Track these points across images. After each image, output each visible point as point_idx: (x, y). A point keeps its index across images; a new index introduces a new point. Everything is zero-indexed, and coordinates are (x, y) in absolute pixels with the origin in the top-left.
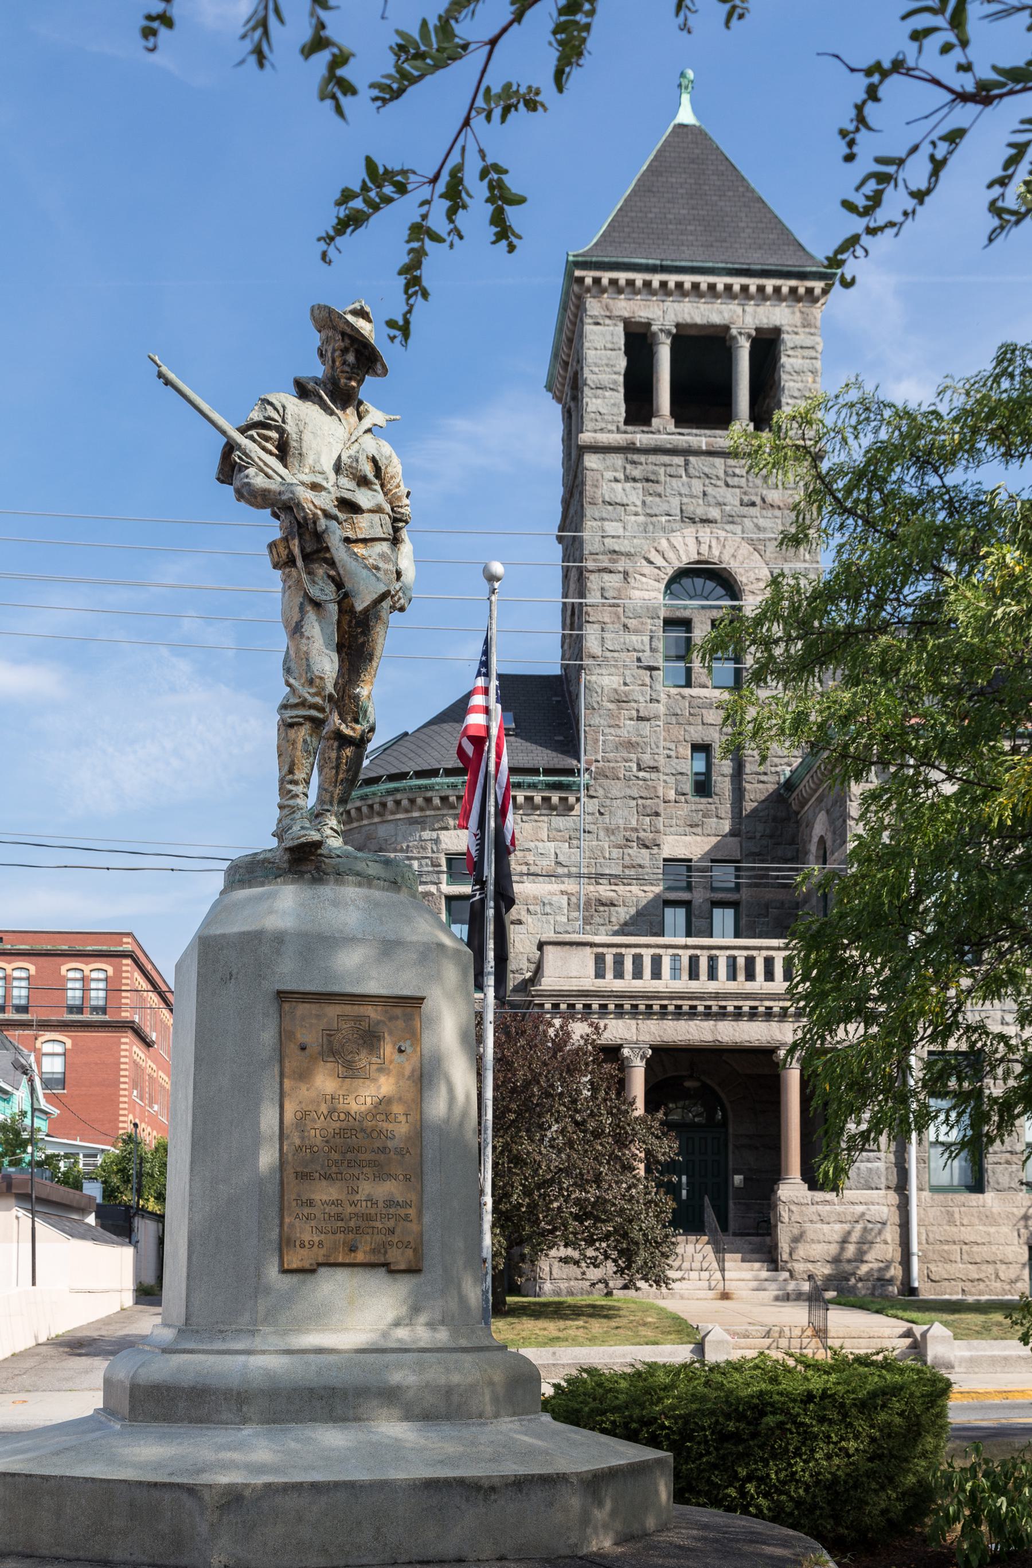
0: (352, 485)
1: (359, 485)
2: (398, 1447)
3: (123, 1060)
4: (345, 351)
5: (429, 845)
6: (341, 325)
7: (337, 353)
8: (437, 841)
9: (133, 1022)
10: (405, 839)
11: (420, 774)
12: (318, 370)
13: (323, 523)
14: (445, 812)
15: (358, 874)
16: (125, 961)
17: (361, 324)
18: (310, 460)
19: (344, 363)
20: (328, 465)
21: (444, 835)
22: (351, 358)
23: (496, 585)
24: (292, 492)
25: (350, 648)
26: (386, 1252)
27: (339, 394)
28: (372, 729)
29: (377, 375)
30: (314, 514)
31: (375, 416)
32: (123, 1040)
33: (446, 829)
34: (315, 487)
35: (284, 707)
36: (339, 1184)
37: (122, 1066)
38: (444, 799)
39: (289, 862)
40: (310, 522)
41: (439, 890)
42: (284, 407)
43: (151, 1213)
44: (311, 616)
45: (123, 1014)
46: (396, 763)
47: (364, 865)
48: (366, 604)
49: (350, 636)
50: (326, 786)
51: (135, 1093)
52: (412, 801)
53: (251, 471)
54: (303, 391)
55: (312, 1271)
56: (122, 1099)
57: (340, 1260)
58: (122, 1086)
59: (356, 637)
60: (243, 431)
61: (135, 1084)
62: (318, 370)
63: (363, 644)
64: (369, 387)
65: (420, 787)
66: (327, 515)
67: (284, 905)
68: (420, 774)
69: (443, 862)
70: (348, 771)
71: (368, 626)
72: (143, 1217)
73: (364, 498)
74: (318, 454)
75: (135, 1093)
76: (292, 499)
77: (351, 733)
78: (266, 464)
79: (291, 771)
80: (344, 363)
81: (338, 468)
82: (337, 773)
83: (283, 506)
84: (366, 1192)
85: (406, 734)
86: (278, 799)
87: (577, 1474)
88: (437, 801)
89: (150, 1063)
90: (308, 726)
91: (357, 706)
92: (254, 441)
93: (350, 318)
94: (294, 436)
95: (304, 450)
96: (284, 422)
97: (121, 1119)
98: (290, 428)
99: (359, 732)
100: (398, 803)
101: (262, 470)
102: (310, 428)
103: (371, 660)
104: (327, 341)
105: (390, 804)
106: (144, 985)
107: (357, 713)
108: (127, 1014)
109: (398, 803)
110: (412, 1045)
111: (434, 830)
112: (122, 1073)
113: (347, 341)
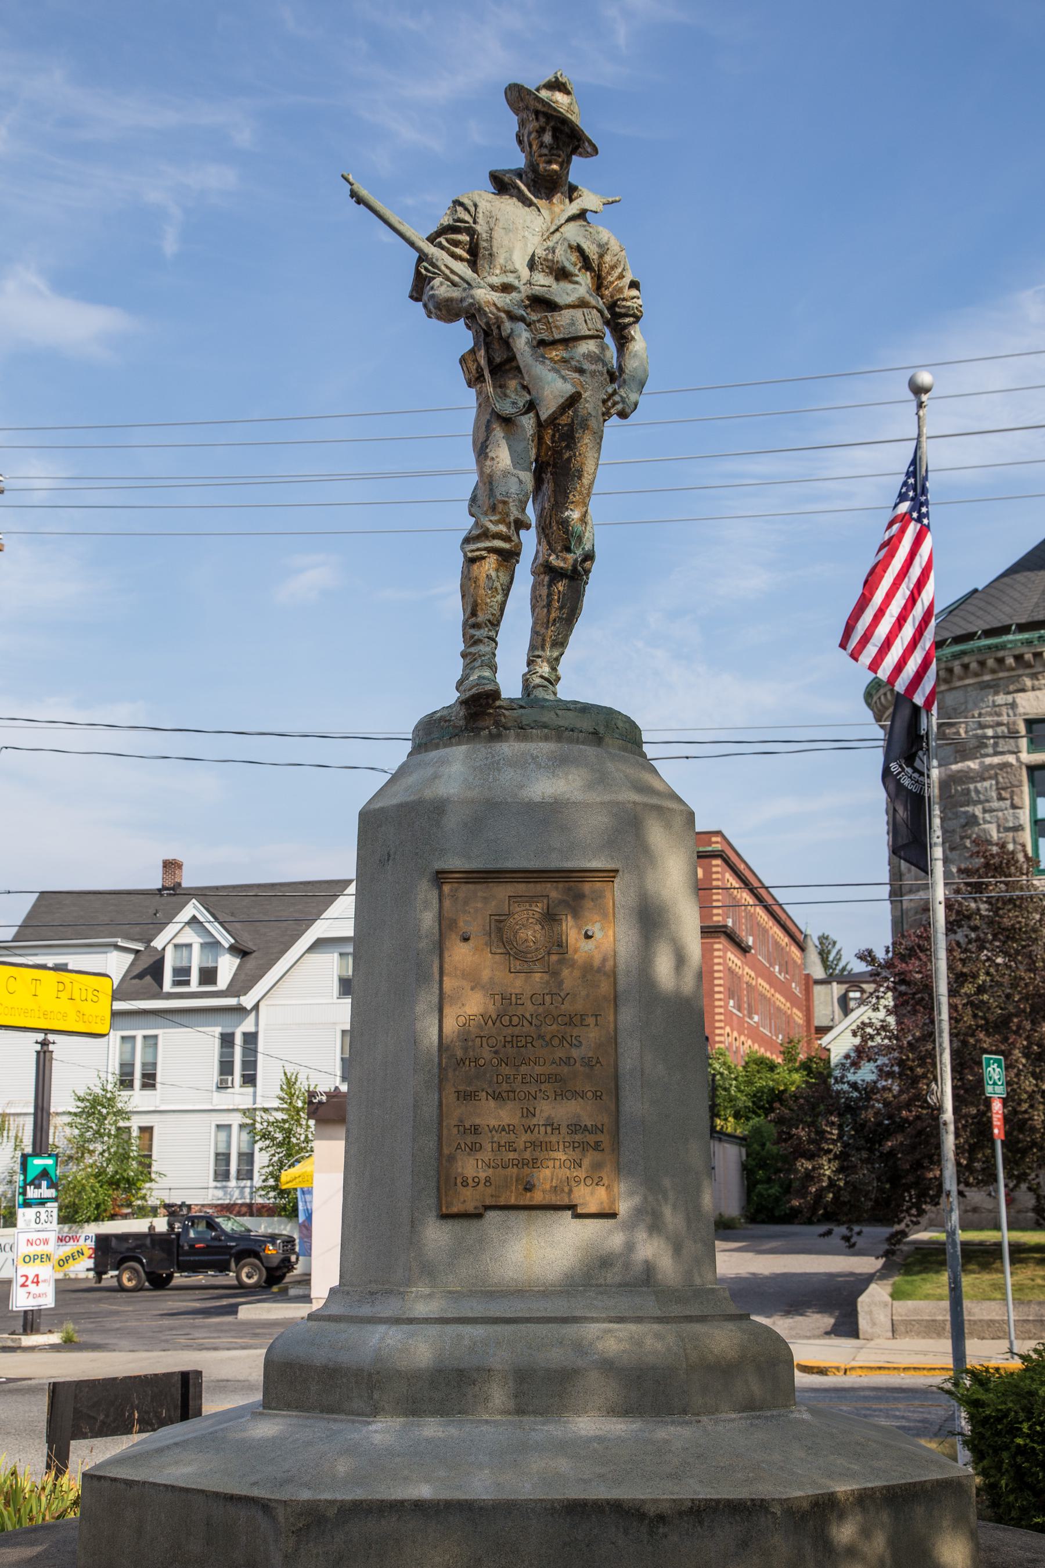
0: (549, 280)
1: (557, 279)
2: (589, 1447)
3: (716, 968)
4: (541, 131)
5: (1004, 710)
6: (533, 104)
7: (533, 136)
8: (1013, 705)
9: (726, 926)
10: (976, 705)
11: (989, 633)
12: (518, 160)
13: (507, 326)
14: (1020, 672)
15: (545, 726)
16: (715, 862)
17: (560, 97)
18: (501, 260)
19: (542, 145)
20: (520, 263)
21: (1020, 698)
22: (547, 138)
23: (924, 398)
24: (472, 297)
25: (554, 466)
26: (571, 1191)
27: (543, 182)
28: (589, 557)
29: (588, 155)
30: (497, 318)
31: (589, 200)
32: (716, 946)
33: (1023, 690)
34: (506, 288)
35: (467, 540)
36: (510, 1105)
37: (716, 975)
38: (1018, 658)
39: (466, 718)
40: (494, 328)
41: (1018, 759)
42: (476, 206)
43: (729, 1135)
44: (498, 433)
45: (715, 918)
46: (962, 623)
47: (552, 715)
48: (550, 412)
49: (555, 452)
50: (538, 629)
51: (731, 1003)
52: (982, 664)
53: (437, 282)
54: (501, 185)
55: (479, 1216)
56: (717, 1010)
57: (513, 1201)
58: (717, 996)
59: (560, 453)
60: (431, 239)
61: (731, 994)
62: (518, 160)
63: (569, 459)
64: (578, 169)
65: (989, 647)
66: (512, 317)
67: (456, 770)
68: (989, 633)
69: (1022, 729)
70: (561, 608)
71: (573, 438)
72: (720, 1140)
73: (564, 293)
74: (510, 251)
75: (731, 1003)
76: (472, 304)
77: (562, 565)
78: (452, 272)
79: (474, 614)
80: (542, 145)
81: (532, 265)
82: (549, 612)
83: (472, 314)
84: (545, 1114)
85: (976, 591)
86: (462, 647)
87: (781, 1501)
88: (1010, 661)
89: (747, 969)
90: (493, 558)
91: (567, 532)
92: (443, 248)
93: (544, 94)
94: (484, 236)
95: (495, 249)
96: (475, 222)
97: (718, 1031)
98: (481, 228)
99: (571, 561)
100: (966, 667)
101: (448, 279)
102: (501, 224)
103: (580, 477)
104: (522, 124)
105: (958, 669)
106: (734, 882)
107: (568, 540)
108: (720, 918)
109: (966, 667)
110: (602, 929)
111: (1009, 693)
112: (717, 982)
113: (542, 120)
